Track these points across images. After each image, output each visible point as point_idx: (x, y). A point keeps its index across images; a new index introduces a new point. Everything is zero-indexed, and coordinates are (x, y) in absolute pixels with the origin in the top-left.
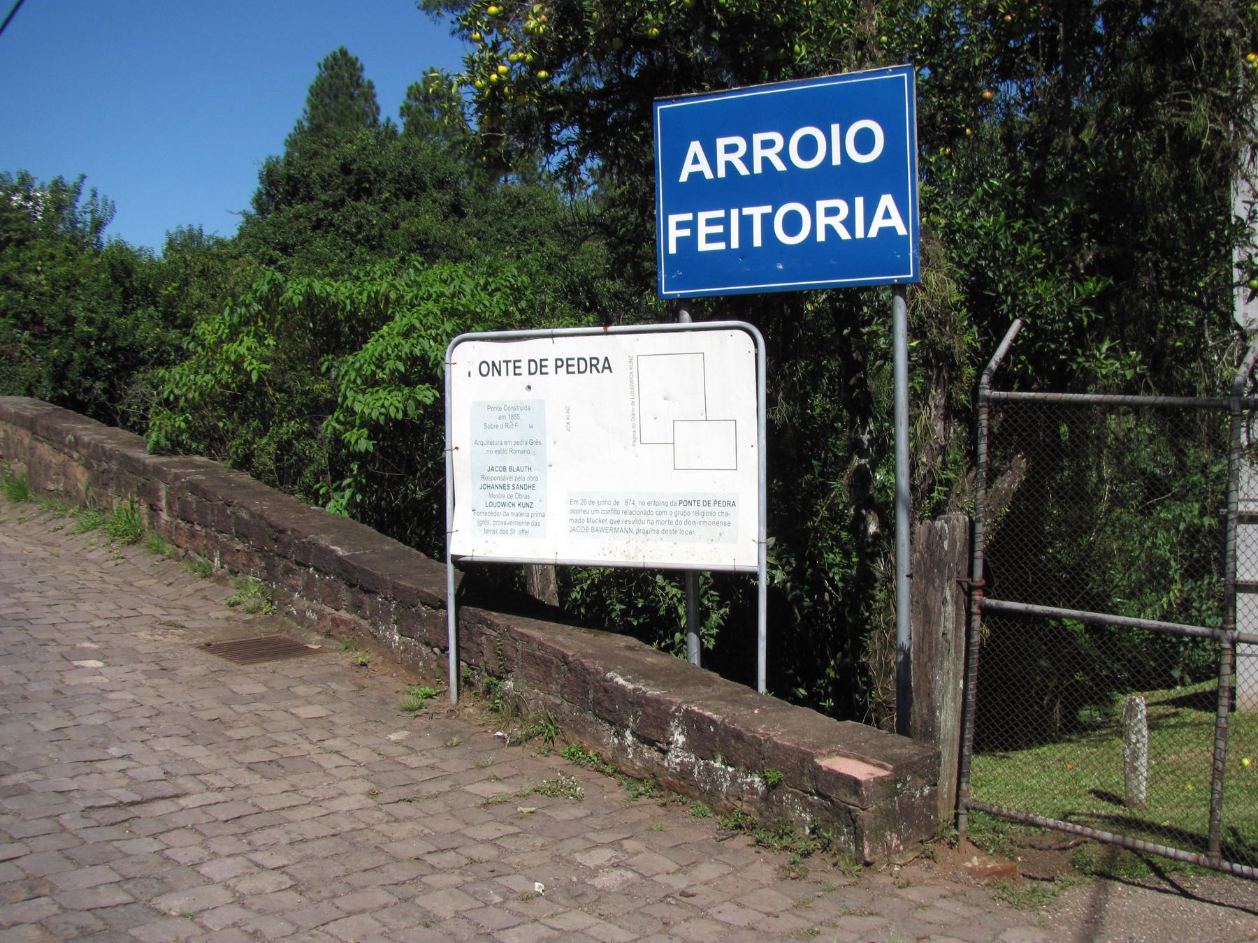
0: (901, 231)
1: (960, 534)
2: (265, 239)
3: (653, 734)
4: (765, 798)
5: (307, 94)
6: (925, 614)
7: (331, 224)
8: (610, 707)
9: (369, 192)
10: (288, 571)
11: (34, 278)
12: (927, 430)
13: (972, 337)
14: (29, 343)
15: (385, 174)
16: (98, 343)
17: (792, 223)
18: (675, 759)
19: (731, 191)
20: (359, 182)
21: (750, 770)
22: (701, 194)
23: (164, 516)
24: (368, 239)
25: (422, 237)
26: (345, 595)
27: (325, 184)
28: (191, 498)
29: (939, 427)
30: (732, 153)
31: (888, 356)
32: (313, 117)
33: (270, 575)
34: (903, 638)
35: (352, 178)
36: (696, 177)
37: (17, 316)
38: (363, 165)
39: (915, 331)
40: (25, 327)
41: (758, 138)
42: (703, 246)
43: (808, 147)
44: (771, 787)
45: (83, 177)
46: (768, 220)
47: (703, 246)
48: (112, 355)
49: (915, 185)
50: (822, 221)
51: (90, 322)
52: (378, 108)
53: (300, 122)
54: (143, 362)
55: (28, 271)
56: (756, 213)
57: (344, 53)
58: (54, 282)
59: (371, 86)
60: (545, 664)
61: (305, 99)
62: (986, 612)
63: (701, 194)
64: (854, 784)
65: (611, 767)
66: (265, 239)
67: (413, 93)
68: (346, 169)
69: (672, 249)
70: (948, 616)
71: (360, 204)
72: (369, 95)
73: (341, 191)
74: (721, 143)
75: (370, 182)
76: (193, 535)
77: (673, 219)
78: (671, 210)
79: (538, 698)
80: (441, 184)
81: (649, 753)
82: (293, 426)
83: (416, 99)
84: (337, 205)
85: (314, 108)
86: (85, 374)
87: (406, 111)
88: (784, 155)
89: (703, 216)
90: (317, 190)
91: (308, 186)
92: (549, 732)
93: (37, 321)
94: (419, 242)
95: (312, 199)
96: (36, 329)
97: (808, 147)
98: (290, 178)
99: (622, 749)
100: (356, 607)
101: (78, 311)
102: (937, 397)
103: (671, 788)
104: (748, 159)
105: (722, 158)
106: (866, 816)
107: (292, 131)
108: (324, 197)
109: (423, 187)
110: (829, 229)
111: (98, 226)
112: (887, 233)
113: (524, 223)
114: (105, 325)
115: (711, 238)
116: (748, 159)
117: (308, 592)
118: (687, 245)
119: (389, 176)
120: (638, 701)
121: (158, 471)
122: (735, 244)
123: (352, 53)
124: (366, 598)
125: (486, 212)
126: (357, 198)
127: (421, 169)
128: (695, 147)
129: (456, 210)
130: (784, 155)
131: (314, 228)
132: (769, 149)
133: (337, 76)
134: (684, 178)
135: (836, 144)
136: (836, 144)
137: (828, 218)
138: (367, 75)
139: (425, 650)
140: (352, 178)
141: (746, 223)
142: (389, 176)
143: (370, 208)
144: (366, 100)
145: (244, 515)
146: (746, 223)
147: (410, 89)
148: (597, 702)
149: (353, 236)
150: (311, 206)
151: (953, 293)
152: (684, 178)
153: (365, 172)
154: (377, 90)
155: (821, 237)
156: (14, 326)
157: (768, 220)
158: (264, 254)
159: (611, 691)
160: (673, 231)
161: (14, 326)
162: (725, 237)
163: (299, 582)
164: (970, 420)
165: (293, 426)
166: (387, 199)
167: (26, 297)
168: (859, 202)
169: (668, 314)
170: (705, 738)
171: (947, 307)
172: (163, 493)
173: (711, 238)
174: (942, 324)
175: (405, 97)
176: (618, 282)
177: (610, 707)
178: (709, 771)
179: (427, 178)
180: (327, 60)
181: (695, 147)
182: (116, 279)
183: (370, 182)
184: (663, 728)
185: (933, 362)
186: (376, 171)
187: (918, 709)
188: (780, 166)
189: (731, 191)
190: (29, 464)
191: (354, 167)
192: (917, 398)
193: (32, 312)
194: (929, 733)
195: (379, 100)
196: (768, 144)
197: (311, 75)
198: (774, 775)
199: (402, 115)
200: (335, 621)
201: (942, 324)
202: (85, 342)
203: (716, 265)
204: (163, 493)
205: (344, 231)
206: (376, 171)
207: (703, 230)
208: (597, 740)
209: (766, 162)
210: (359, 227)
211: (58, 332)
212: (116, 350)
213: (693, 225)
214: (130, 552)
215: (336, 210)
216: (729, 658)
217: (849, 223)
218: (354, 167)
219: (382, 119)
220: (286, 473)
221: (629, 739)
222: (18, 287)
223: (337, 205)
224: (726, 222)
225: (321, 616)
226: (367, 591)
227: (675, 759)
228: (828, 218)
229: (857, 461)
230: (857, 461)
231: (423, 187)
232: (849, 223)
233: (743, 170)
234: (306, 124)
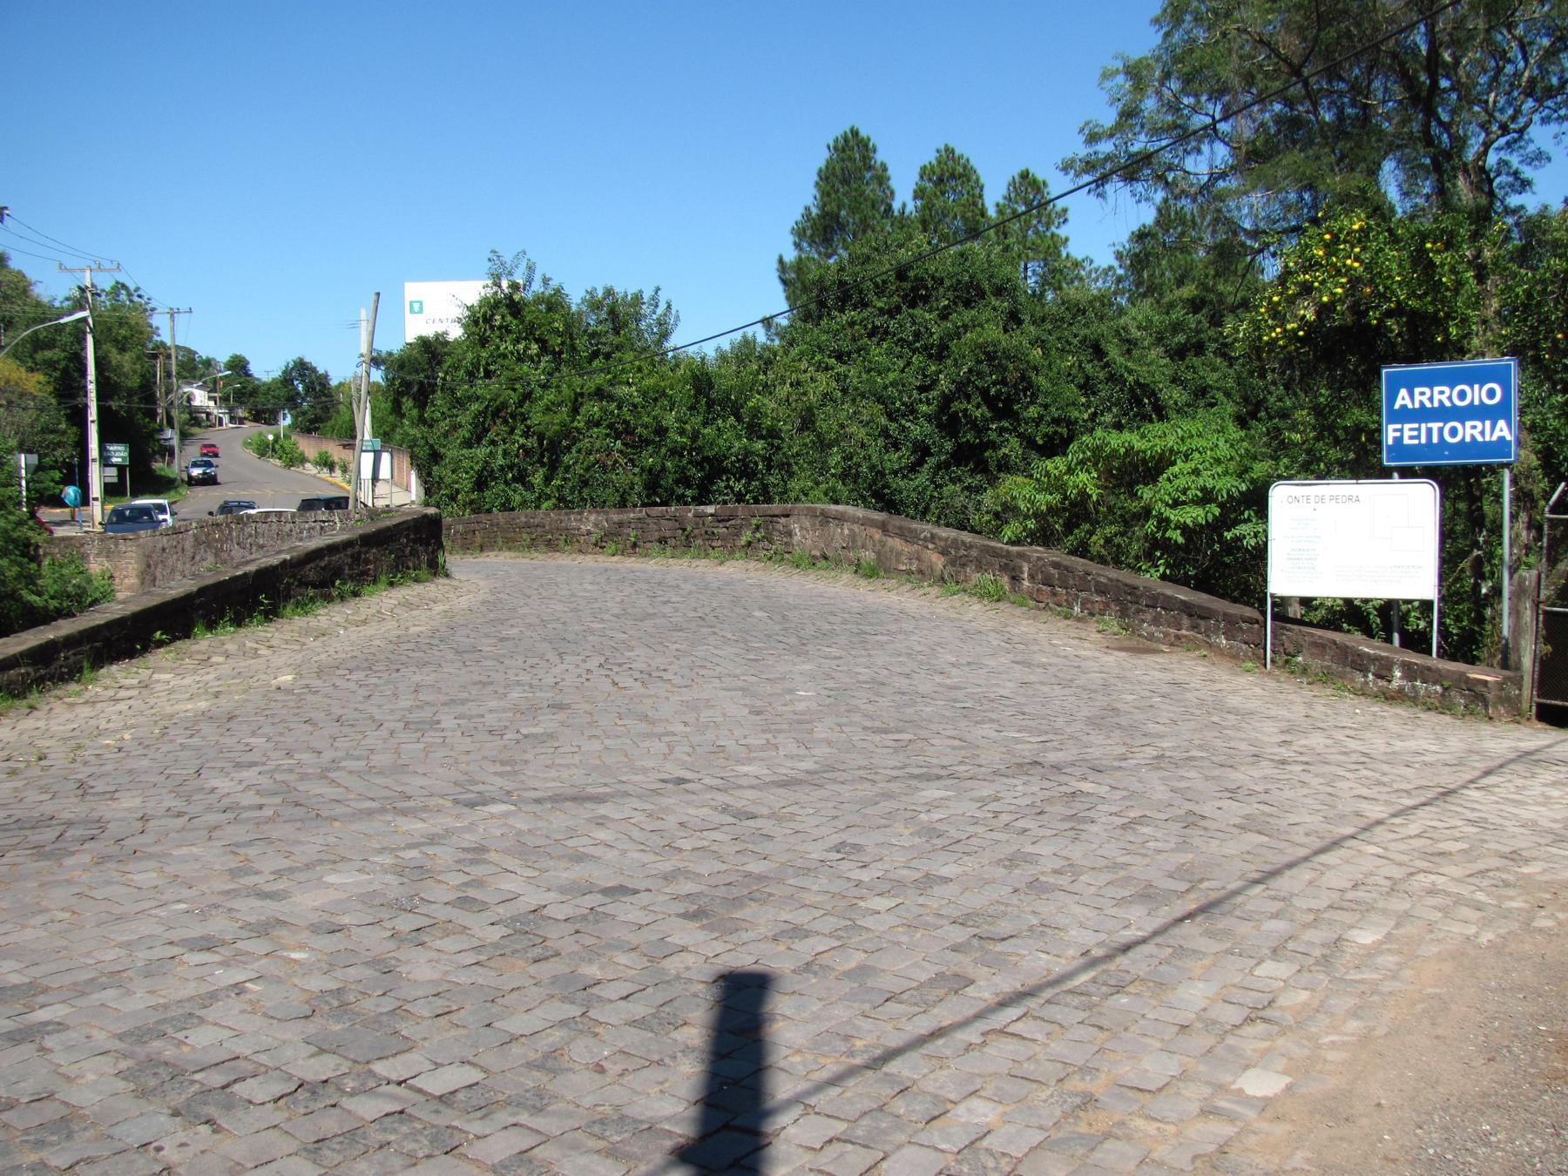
0: (1508, 438)
1: (1534, 579)
2: (819, 347)
3: (1384, 673)
4: (1442, 695)
5: (816, 178)
6: (1516, 613)
7: (886, 332)
8: (1359, 663)
9: (926, 299)
10: (1138, 611)
11: (626, 389)
12: (1517, 536)
13: (1544, 484)
14: (621, 452)
15: (941, 282)
16: (690, 453)
17: (1453, 432)
18: (1395, 684)
19: (1422, 415)
20: (914, 289)
21: (1435, 683)
22: (1405, 415)
23: (1026, 583)
24: (926, 348)
25: (990, 349)
26: (1186, 621)
27: (880, 291)
28: (1052, 571)
29: (1524, 533)
30: (1422, 396)
31: (1498, 497)
32: (824, 205)
33: (1123, 613)
34: (1505, 632)
35: (906, 285)
36: (1404, 407)
37: (611, 426)
38: (920, 272)
39: (1514, 481)
40: (617, 436)
41: (1437, 389)
42: (1406, 441)
43: (1462, 395)
44: (1445, 689)
45: (658, 289)
46: (1441, 430)
47: (1406, 441)
48: (699, 465)
49: (1515, 417)
50: (1469, 432)
51: (682, 433)
52: (892, 193)
53: (807, 209)
54: (726, 471)
55: (620, 383)
56: (1435, 426)
57: (855, 133)
58: (644, 394)
59: (885, 169)
60: (1320, 647)
61: (812, 184)
62: (1545, 612)
63: (1405, 415)
64: (1485, 683)
65: (1362, 692)
66: (819, 347)
67: (924, 173)
68: (901, 274)
69: (1390, 442)
70: (1528, 615)
71: (917, 312)
72: (882, 179)
73: (896, 298)
74: (1417, 390)
75: (926, 288)
76: (1054, 594)
77: (1391, 427)
78: (1389, 422)
79: (1316, 664)
80: (999, 291)
81: (1381, 683)
82: (1114, 529)
83: (930, 180)
84: (892, 312)
85: (825, 194)
86: (677, 482)
87: (919, 194)
88: (1450, 398)
89: (1407, 426)
90: (871, 296)
91: (861, 292)
92: (1326, 678)
93: (629, 430)
94: (987, 354)
95: (865, 305)
96: (628, 439)
97: (1462, 395)
98: (842, 284)
99: (1366, 683)
100: (1194, 627)
101: (670, 419)
102: (1523, 517)
103: (1393, 698)
104: (1431, 399)
105: (1417, 398)
106: (1490, 696)
107: (799, 218)
108: (880, 305)
109: (982, 294)
110: (1473, 437)
111: (665, 335)
112: (1502, 439)
113: (1082, 332)
114: (695, 436)
115: (1411, 438)
116: (1431, 399)
117: (1156, 621)
118: (1398, 440)
119: (947, 283)
120: (1376, 659)
121: (1021, 555)
122: (1423, 441)
123: (863, 133)
124: (1202, 623)
125: (1043, 320)
126: (913, 305)
127: (980, 276)
128: (1403, 392)
129: (1014, 317)
130: (1450, 398)
131: (871, 335)
132: (1442, 395)
133: (850, 159)
134: (1397, 407)
135: (1477, 394)
136: (1477, 394)
137: (1471, 431)
138: (880, 157)
139: (1244, 647)
140: (906, 285)
141: (1429, 431)
142: (947, 283)
143: (927, 316)
144: (880, 184)
145: (1102, 580)
146: (1429, 431)
147: (923, 169)
148: (1353, 661)
149: (910, 344)
150: (865, 314)
151: (1534, 461)
152: (1397, 407)
153: (922, 279)
154: (890, 172)
155: (1468, 439)
156: (608, 435)
157: (1441, 430)
158: (820, 362)
159: (1361, 655)
160: (1390, 433)
161: (608, 435)
162: (1418, 437)
163: (1148, 617)
164: (1539, 529)
165: (1114, 529)
166: (946, 307)
167: (620, 408)
168: (1488, 423)
169: (1385, 474)
170: (1410, 672)
171: (1530, 469)
172: (1026, 569)
173: (1411, 438)
174: (1527, 477)
175: (917, 178)
176: (1363, 460)
177: (1359, 663)
178: (1414, 687)
179: (986, 286)
180: (836, 140)
181: (1403, 392)
182: (699, 391)
183: (926, 288)
184: (1390, 670)
185: (1524, 498)
186: (933, 278)
187: (1513, 658)
188: (1448, 404)
189: (1422, 415)
190: (878, 553)
191: (911, 274)
192: (1514, 517)
193: (626, 422)
194: (1518, 667)
195: (893, 184)
196: (1442, 393)
197: (820, 158)
198: (1446, 684)
199: (915, 198)
200: (1178, 637)
201: (1527, 477)
202: (676, 452)
203: (1413, 451)
204: (1026, 569)
205: (901, 339)
206: (933, 278)
207: (1407, 434)
208: (1352, 680)
209: (1440, 402)
210: (917, 335)
211: (653, 442)
212: (706, 459)
213: (1401, 430)
214: (1000, 605)
215: (892, 317)
216: (1416, 642)
217: (1482, 433)
218: (911, 274)
219: (896, 206)
220: (1116, 557)
221: (1371, 677)
222: (611, 398)
223: (892, 312)
224: (1418, 429)
225: (1166, 635)
226: (1201, 617)
227: (1395, 684)
228: (1471, 431)
229: (1476, 553)
230: (1476, 553)
231: (982, 294)
232: (1482, 433)
233: (1428, 405)
234: (814, 211)
